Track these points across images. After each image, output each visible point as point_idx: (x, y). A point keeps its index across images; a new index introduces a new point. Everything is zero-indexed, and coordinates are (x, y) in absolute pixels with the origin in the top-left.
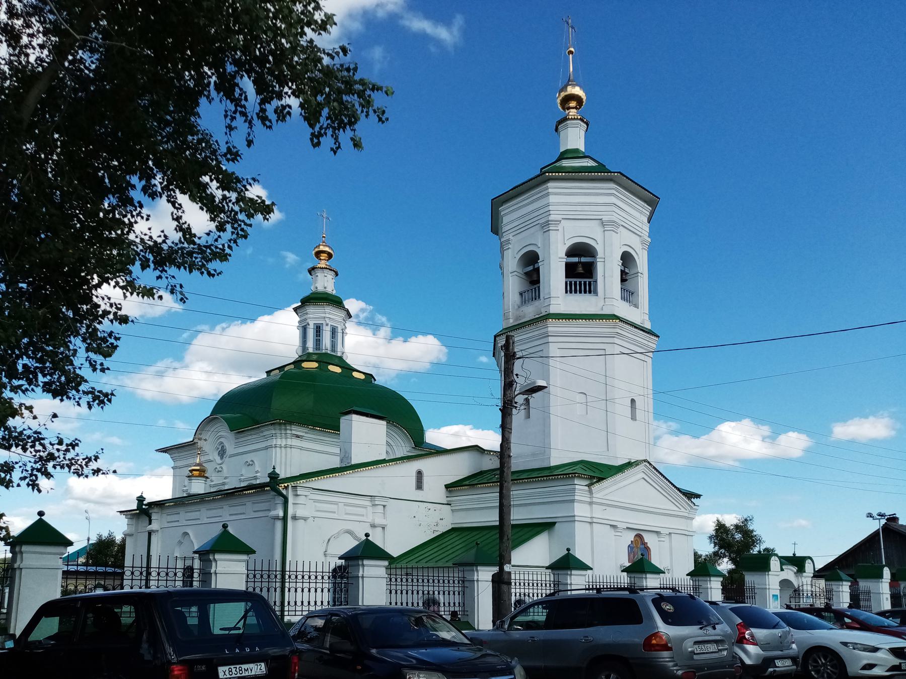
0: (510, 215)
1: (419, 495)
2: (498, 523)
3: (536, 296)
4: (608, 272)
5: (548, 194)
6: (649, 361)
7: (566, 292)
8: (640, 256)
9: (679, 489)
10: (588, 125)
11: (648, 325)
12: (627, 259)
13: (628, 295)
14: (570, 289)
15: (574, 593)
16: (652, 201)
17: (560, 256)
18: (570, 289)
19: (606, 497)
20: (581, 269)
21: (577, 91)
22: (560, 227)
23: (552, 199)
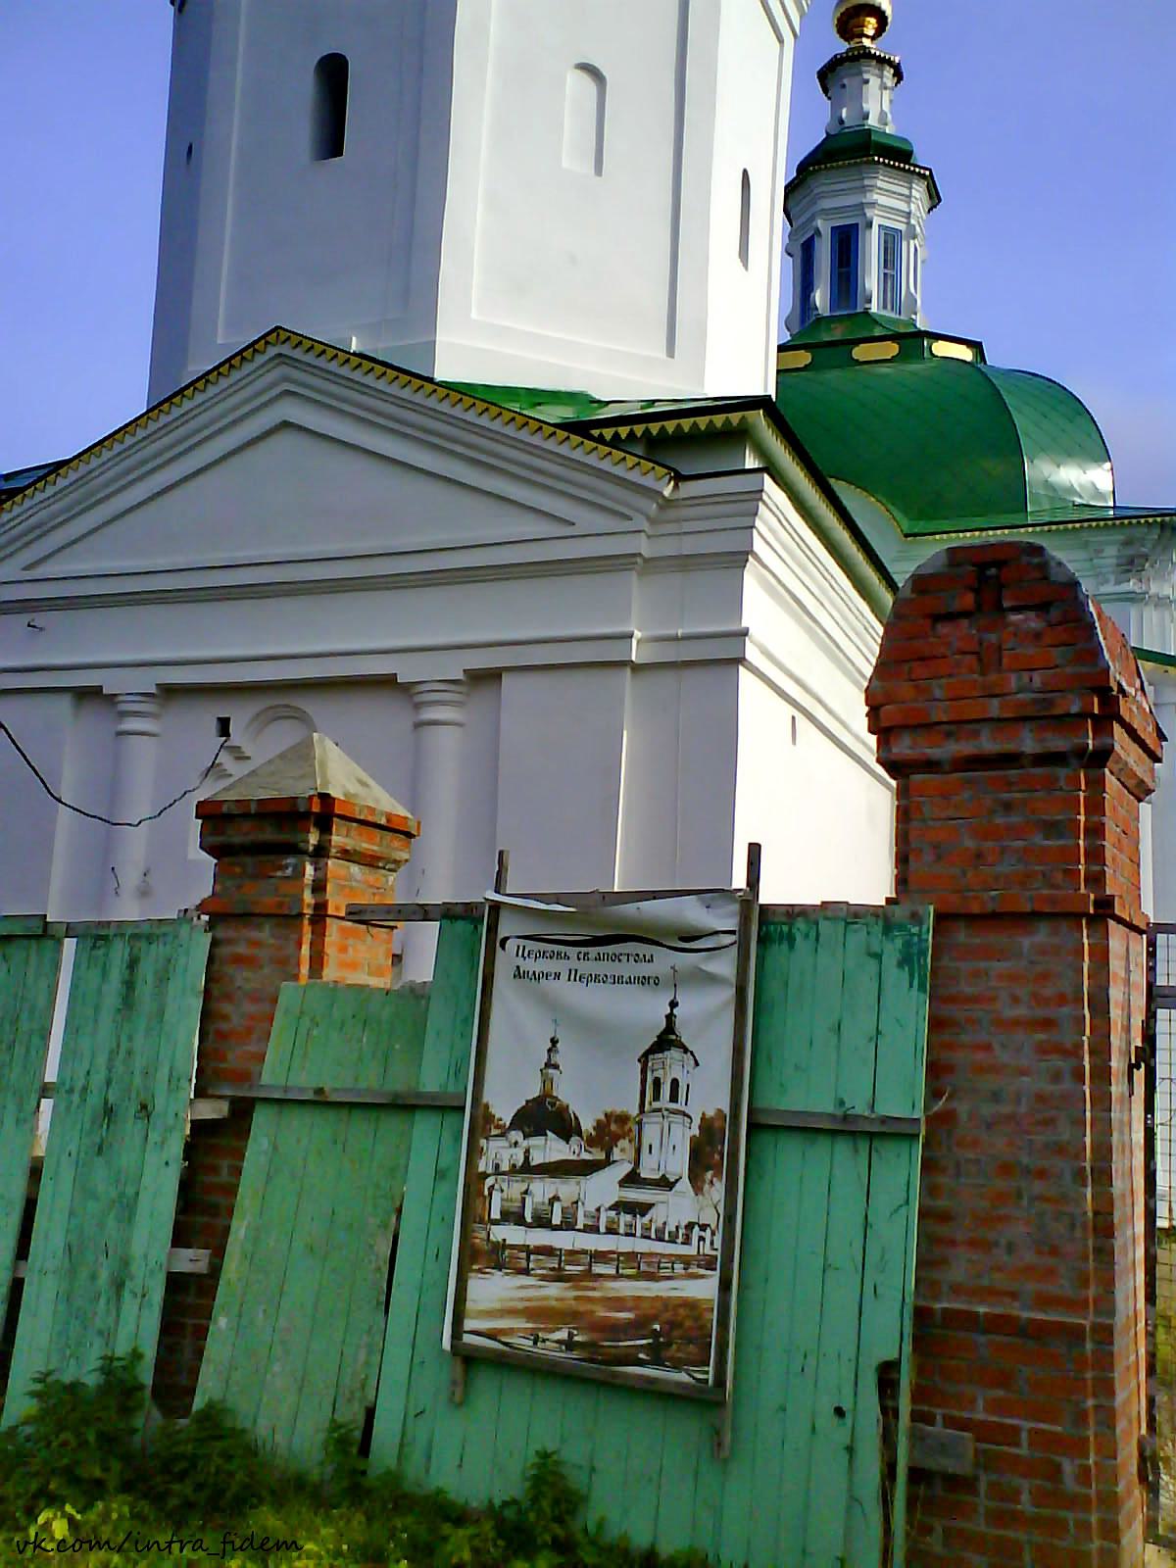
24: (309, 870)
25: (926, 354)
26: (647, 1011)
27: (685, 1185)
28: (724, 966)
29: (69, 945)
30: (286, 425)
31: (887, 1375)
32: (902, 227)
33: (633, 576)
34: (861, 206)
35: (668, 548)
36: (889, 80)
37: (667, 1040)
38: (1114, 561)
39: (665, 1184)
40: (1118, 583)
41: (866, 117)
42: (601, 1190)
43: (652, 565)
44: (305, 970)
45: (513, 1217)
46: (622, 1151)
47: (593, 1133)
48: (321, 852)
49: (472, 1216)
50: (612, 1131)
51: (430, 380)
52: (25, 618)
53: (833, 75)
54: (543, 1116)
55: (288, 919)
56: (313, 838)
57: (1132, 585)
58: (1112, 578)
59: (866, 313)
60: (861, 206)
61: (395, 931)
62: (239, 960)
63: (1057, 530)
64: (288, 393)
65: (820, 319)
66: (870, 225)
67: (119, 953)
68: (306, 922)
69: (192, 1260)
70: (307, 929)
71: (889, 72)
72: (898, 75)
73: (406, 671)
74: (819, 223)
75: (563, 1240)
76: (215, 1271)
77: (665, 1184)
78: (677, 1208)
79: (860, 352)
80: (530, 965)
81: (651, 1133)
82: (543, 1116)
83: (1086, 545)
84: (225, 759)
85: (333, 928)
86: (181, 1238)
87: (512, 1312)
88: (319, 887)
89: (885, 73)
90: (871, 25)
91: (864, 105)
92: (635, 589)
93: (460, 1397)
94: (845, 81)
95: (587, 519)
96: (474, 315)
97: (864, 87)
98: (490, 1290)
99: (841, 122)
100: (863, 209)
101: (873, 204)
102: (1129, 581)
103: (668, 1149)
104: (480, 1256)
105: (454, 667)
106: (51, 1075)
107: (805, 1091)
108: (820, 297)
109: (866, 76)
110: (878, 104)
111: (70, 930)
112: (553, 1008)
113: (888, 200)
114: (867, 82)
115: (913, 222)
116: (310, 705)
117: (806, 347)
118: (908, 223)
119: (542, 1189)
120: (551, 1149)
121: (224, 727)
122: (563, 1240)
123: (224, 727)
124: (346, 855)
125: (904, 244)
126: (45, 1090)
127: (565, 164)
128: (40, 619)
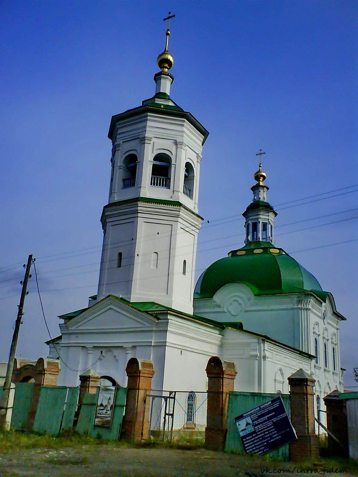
0: (123, 131)
1: (181, 350)
2: (34, 365)
3: (132, 184)
4: (178, 174)
5: (178, 216)
6: (196, 235)
7: (151, 184)
8: (196, 167)
9: (105, 233)
10: (173, 79)
11: (196, 212)
12: (189, 167)
13: (189, 191)
14: (153, 183)
15: (284, 307)
16: (204, 133)
17: (149, 159)
18: (153, 183)
19: (80, 328)
20: (162, 170)
21: (170, 58)
22: (151, 142)
23: (149, 123)
24: (88, 382)
25: (269, 252)
26: (108, 396)
27: (110, 411)
28: (114, 392)
29: (68, 389)
30: (111, 308)
31: (120, 424)
32: (267, 222)
33: (153, 333)
34: (258, 218)
35: (157, 329)
36: (266, 190)
37: (110, 399)
38: (296, 301)
39: (108, 410)
40: (297, 306)
41: (260, 198)
42: (105, 411)
43: (156, 331)
44: (87, 392)
45: (99, 414)
46: (106, 408)
47: (324, 439)
48: (89, 381)
49: (96, 414)
50: (106, 406)
51: (130, 302)
52: (76, 335)
53: (255, 189)
54: (102, 405)
55: (86, 387)
56: (88, 379)
57: (300, 306)
58: (296, 304)
59: (259, 241)
60: (258, 218)
61: (152, 378)
62: (82, 391)
63: (284, 295)
64: (111, 304)
65: (250, 242)
66: (259, 222)
67: (72, 390)
68: (257, 350)
69: (76, 419)
70: (88, 388)
71: (265, 189)
72: (268, 189)
73: (125, 345)
74: (249, 222)
75: (102, 415)
76: (78, 419)
77: (108, 410)
78: (109, 412)
79: (256, 251)
80: (102, 392)
81: (108, 407)
82: (102, 405)
83: (290, 298)
84: (101, 357)
85: (90, 388)
86: (75, 417)
87: (98, 422)
88: (89, 383)
89: (264, 189)
90: (261, 179)
91: (260, 196)
92: (154, 334)
93: (94, 429)
94: (256, 191)
95: (147, 325)
96: (137, 292)
97: (260, 192)
98: (97, 420)
99: (255, 199)
100: (258, 219)
101: (260, 218)
102: (299, 305)
103: (109, 408)
104: (97, 417)
105: (130, 345)
106: (66, 402)
107: (118, 403)
108: (250, 238)
109: (260, 190)
110: (263, 196)
111: (68, 387)
112: (103, 396)
113: (263, 217)
114: (260, 191)
115: (269, 220)
116: (112, 349)
117: (245, 250)
118: (269, 221)
119: (101, 411)
120: (102, 408)
121: (102, 352)
122: (102, 415)
123: (102, 352)
124: (92, 381)
125: (268, 225)
126: (65, 403)
127: (152, 267)
128: (77, 335)
